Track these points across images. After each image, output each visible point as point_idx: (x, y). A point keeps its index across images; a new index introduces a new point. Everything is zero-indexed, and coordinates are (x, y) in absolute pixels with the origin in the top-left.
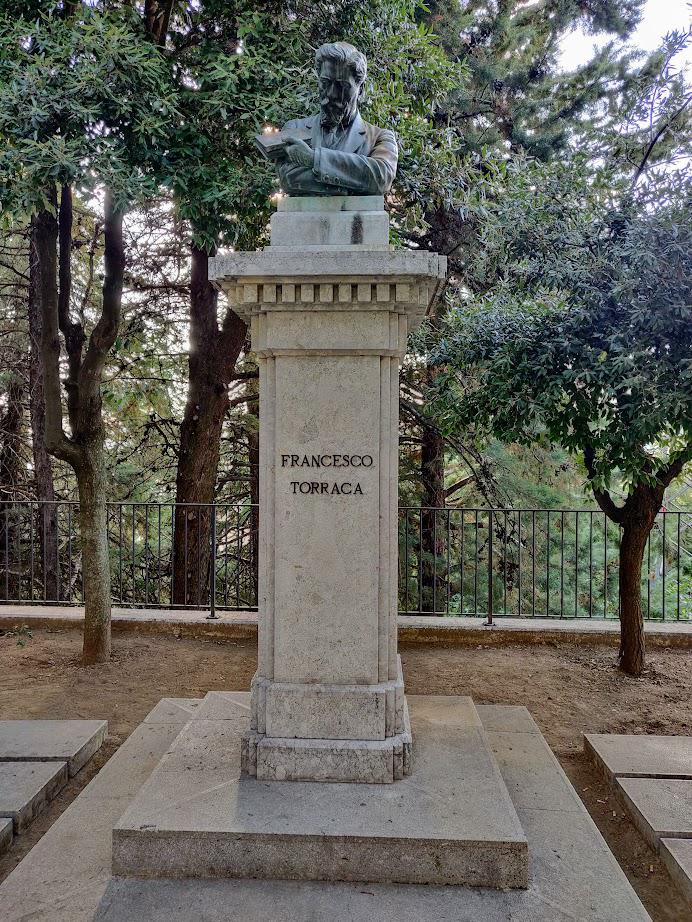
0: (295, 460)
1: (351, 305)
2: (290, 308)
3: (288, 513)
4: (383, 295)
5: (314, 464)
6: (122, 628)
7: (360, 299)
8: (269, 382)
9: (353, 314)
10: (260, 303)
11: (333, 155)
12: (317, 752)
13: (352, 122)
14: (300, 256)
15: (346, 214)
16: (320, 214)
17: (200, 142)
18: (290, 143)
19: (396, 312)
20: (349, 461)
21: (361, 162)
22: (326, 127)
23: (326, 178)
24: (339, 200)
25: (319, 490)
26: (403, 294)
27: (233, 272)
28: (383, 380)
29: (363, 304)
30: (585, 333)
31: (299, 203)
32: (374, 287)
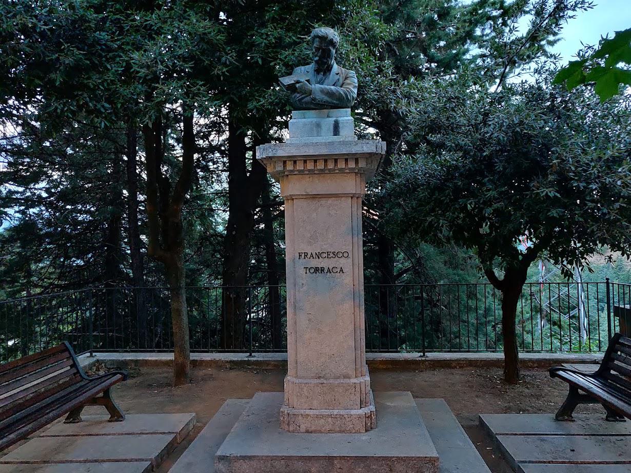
2: (301, 172)
3: (303, 284)
6: (194, 363)
12: (322, 416)
13: (332, 68)
14: (306, 145)
15: (330, 119)
18: (298, 82)
20: (335, 254)
21: (337, 91)
22: (317, 71)
30: (470, 175)
31: (304, 114)
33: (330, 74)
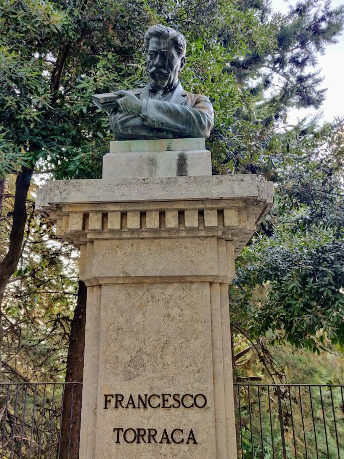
0: (119, 399)
1: (177, 230)
4: (211, 220)
5: (142, 406)
7: (187, 224)
8: (95, 309)
9: (180, 240)
10: (86, 231)
11: (160, 105)
13: (175, 88)
16: (147, 154)
17: (71, 134)
19: (223, 237)
20: (180, 401)
23: (153, 121)
24: (165, 142)
25: (146, 438)
26: (231, 219)
27: (57, 200)
28: (214, 308)
29: (191, 229)
32: (201, 213)
33: (172, 95)
